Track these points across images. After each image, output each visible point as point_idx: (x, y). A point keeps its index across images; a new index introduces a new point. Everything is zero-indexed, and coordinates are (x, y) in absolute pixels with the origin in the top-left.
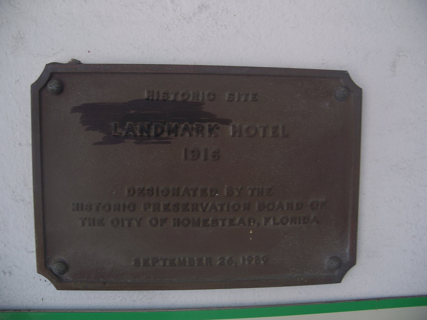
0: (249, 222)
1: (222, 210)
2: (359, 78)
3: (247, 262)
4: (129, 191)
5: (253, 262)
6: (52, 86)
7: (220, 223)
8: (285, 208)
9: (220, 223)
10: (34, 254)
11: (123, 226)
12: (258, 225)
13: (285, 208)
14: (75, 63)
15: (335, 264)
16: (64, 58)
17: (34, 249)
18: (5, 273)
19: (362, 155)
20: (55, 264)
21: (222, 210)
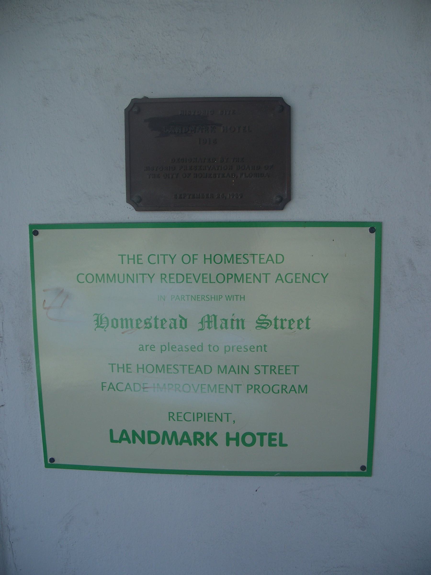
0: (232, 175)
1: (218, 169)
2: (291, 99)
3: (231, 197)
4: (172, 160)
5: (235, 197)
6: (135, 110)
7: (217, 176)
8: (251, 169)
9: (217, 176)
10: (125, 194)
11: (169, 177)
12: (237, 177)
13: (251, 169)
14: (145, 98)
15: (278, 199)
16: (140, 96)
17: (125, 192)
18: (110, 204)
19: (179, 212)
20: (139, 197)
21: (218, 169)
